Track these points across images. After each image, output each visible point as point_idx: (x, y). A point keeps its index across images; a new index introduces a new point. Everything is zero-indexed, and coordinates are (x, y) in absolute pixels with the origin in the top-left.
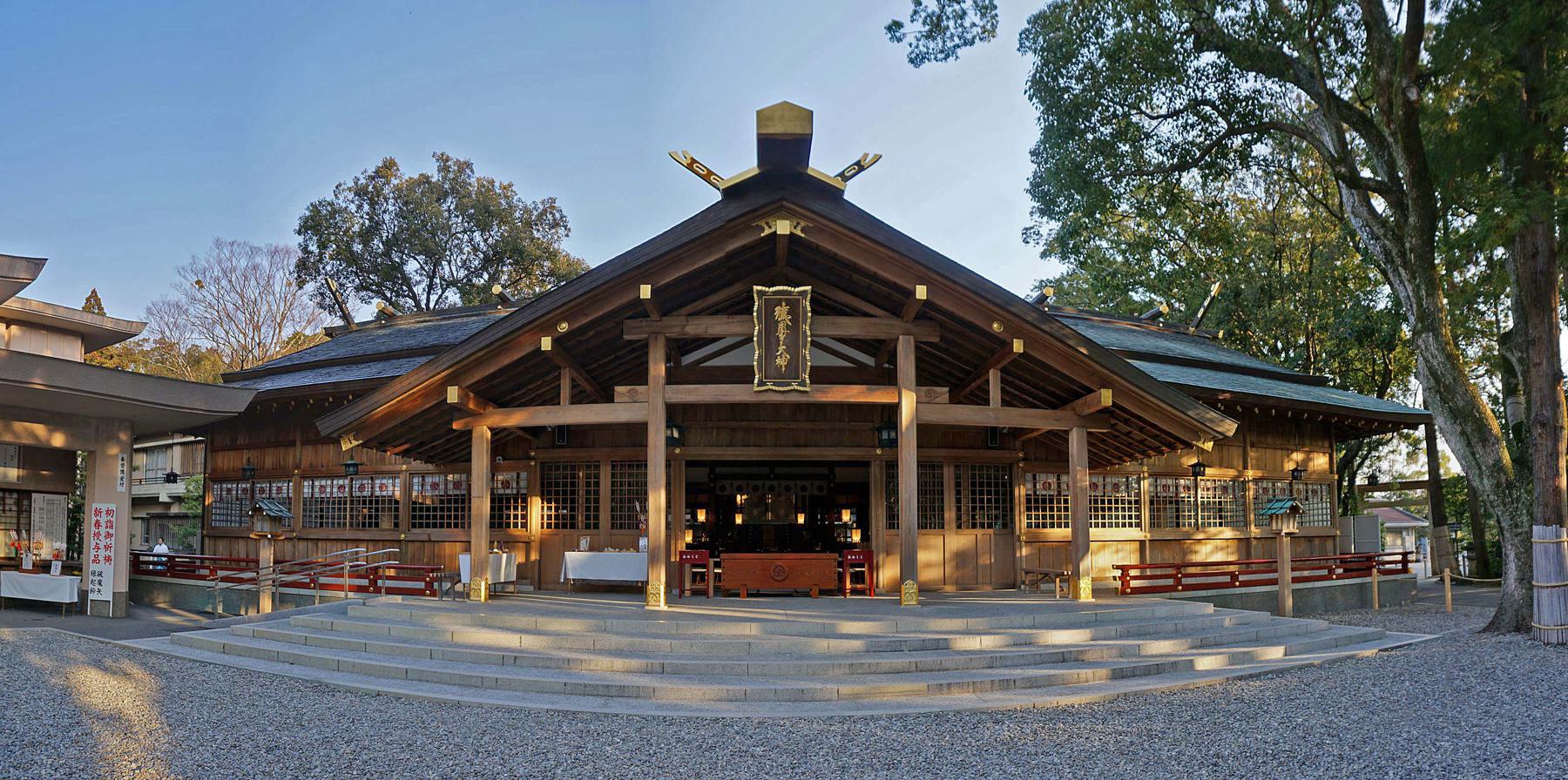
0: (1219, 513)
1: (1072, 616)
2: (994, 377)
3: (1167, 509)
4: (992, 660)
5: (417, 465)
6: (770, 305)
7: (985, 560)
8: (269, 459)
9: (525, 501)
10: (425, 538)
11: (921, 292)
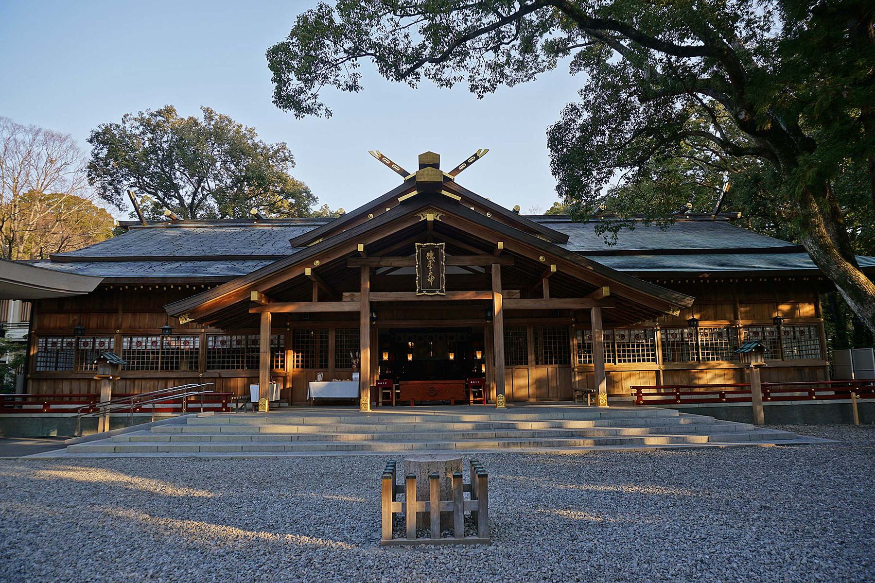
0: (714, 350)
1: (593, 415)
2: (545, 284)
3: (675, 351)
4: (535, 434)
5: (213, 330)
6: (424, 252)
7: (553, 384)
8: (94, 321)
9: (283, 351)
10: (217, 375)
11: (501, 245)
